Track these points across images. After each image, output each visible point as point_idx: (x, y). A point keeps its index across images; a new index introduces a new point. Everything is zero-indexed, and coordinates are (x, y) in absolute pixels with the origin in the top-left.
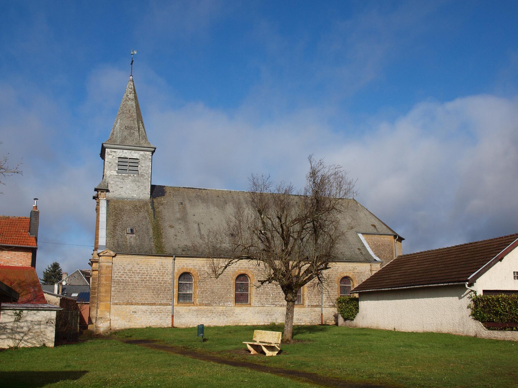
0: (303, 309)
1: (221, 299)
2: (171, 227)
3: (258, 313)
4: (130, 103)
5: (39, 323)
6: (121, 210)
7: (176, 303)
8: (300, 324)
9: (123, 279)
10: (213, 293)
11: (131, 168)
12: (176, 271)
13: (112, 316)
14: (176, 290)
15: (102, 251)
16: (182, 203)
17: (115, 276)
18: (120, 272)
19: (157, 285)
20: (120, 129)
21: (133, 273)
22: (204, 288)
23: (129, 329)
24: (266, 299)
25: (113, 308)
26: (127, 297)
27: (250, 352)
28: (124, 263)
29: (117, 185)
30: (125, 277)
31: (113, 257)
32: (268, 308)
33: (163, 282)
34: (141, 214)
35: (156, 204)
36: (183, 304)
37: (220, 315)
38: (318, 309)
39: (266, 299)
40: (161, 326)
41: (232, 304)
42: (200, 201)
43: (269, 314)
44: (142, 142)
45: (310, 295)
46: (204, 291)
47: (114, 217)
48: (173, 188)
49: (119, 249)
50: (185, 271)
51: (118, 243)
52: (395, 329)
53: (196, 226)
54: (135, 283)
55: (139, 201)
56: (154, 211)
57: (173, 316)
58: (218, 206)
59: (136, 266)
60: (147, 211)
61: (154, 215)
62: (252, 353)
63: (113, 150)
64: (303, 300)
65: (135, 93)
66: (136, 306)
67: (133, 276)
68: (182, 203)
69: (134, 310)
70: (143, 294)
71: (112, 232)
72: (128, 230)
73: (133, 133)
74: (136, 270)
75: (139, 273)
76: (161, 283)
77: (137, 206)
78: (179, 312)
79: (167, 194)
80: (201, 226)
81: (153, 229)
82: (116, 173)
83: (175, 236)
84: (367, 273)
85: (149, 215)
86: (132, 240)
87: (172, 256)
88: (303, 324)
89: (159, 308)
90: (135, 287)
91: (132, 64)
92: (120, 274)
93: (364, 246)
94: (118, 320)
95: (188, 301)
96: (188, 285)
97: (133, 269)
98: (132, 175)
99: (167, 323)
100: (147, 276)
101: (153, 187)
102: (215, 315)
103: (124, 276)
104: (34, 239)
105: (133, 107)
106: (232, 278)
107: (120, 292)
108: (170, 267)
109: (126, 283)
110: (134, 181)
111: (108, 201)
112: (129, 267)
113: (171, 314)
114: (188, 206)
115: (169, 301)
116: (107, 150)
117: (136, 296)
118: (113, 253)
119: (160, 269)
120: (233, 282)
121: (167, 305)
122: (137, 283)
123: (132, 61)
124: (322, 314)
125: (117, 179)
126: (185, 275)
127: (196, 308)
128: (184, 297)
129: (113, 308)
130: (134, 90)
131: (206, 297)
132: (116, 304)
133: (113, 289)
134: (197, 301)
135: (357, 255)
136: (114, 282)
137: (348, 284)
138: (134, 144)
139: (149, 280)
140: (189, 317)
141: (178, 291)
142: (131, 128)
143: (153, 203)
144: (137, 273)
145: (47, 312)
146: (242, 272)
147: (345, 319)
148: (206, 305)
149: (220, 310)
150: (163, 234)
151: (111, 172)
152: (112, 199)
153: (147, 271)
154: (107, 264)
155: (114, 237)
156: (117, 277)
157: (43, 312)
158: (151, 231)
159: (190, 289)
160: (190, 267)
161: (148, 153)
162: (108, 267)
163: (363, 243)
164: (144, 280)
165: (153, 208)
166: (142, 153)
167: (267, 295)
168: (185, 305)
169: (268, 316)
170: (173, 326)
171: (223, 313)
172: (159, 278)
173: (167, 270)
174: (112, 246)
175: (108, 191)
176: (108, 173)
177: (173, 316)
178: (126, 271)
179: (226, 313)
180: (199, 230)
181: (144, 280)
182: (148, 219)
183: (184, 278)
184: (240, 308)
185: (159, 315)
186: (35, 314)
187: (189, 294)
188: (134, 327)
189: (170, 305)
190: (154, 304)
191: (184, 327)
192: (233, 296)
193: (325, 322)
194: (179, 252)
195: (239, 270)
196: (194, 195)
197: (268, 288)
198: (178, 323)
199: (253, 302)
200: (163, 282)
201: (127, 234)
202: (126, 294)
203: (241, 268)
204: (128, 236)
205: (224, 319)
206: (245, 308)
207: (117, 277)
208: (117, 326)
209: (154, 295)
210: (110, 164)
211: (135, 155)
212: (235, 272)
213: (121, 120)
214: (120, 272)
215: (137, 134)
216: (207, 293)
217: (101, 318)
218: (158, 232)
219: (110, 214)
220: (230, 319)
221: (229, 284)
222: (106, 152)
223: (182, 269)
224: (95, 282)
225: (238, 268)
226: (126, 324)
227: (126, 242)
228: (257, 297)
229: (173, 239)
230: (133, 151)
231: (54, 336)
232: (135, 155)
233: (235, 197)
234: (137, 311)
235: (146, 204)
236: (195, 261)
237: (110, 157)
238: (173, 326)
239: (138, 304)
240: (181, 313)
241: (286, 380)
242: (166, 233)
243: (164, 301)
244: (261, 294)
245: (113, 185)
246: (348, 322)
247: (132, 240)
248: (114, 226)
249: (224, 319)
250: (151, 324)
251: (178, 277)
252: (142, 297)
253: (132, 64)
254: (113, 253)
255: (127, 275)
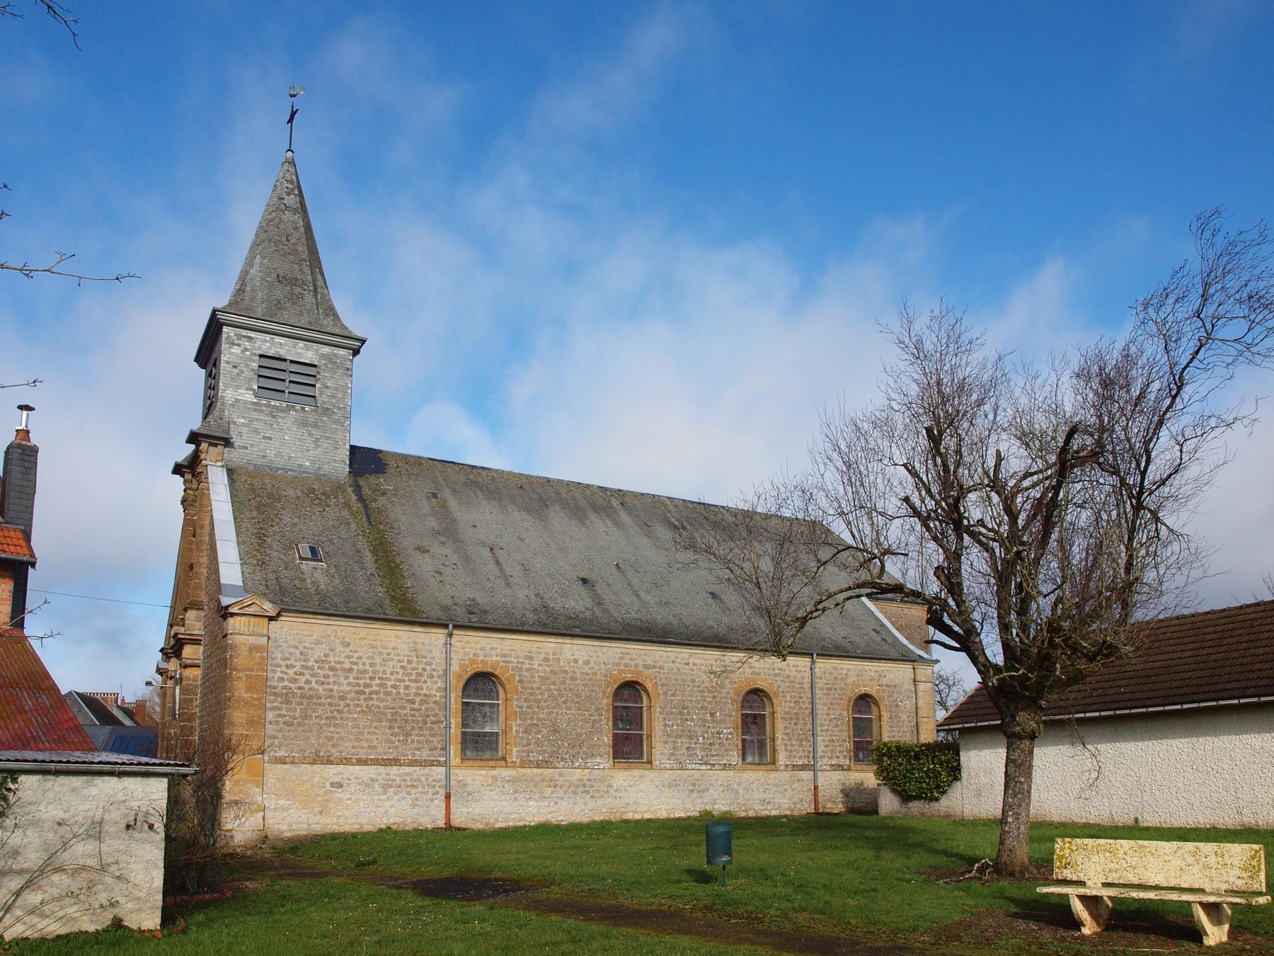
0: (773, 775)
1: (577, 750)
2: (422, 550)
3: (670, 786)
4: (288, 216)
5: (96, 830)
6: (270, 496)
7: (458, 760)
8: (767, 813)
9: (300, 688)
10: (555, 731)
11: (295, 388)
12: (455, 667)
13: (272, 803)
14: (455, 721)
15: (233, 600)
16: (435, 496)
17: (278, 677)
18: (293, 666)
19: (402, 708)
20: (262, 279)
21: (332, 669)
22: (532, 719)
23: (334, 837)
24: (688, 748)
25: (273, 773)
26: (313, 740)
27: (1077, 924)
28: (300, 637)
29: (256, 431)
30: (308, 682)
31: (271, 619)
32: (695, 772)
33: (418, 699)
34: (332, 513)
35: (366, 491)
36: (477, 763)
37: (575, 793)
38: (807, 775)
39: (688, 748)
40: (415, 825)
41: (604, 761)
42: (479, 493)
43: (696, 788)
44: (327, 323)
45: (790, 739)
46: (532, 725)
47: (255, 514)
48: (405, 458)
49: (291, 601)
50: (481, 668)
51: (279, 583)
52: (1136, 820)
53: (486, 553)
54: (337, 701)
55: (319, 478)
56: (366, 507)
57: (448, 797)
58: (527, 510)
59: (339, 648)
60: (347, 505)
61: (370, 522)
62: (1086, 931)
63: (244, 332)
64: (774, 751)
65: (301, 195)
66: (340, 768)
67: (331, 680)
68: (435, 496)
69: (336, 780)
70: (362, 733)
71: (256, 549)
72: (305, 549)
73: (301, 296)
74: (339, 663)
75: (350, 670)
76: (413, 702)
77: (316, 492)
78: (465, 785)
79: (391, 470)
80: (499, 553)
81: (374, 552)
82: (250, 397)
83: (433, 572)
84: (906, 686)
85: (352, 514)
86: (318, 575)
87: (446, 626)
88: (774, 813)
89: (408, 774)
90: (340, 712)
91: (291, 121)
92: (291, 672)
93: (883, 625)
94: (287, 809)
95: (488, 755)
96: (487, 709)
97: (331, 659)
98: (298, 407)
99: (430, 815)
100: (372, 678)
101: (352, 447)
102: (561, 793)
103: (303, 679)
104: (20, 536)
105: (296, 229)
106: (604, 692)
107: (291, 724)
108: (438, 655)
109: (310, 698)
110: (304, 423)
111: (231, 472)
112: (319, 652)
113: (442, 792)
114: (453, 504)
115: (436, 753)
116: (225, 329)
117: (342, 739)
118: (270, 609)
119: (409, 662)
120: (606, 702)
121: (431, 764)
122: (343, 698)
123: (293, 114)
124: (816, 788)
125: (255, 415)
126: (482, 682)
127: (513, 772)
128: (479, 745)
129: (273, 773)
130: (299, 188)
131: (537, 743)
132: (282, 761)
133: (270, 715)
134: (515, 753)
135: (875, 642)
136: (275, 694)
137: (865, 713)
138: (303, 323)
139: (377, 693)
140: (496, 800)
141: (464, 725)
142: (294, 282)
143: (358, 489)
144: (344, 670)
145: (129, 782)
146: (629, 677)
147: (906, 797)
148: (538, 766)
149: (574, 779)
150: (405, 567)
151: (238, 392)
152: (241, 468)
153: (372, 665)
154: (252, 640)
155: (262, 564)
156: (282, 679)
157: (113, 781)
158: (369, 558)
159: (492, 719)
160: (494, 658)
161: (342, 352)
162: (253, 649)
163: (877, 619)
164: (363, 693)
165: (361, 499)
166: (326, 350)
167: (690, 738)
168: (482, 763)
169: (695, 795)
170: (449, 826)
171: (583, 788)
172: (407, 687)
173: (431, 664)
174: (263, 588)
175: (227, 443)
176: (228, 393)
177: (448, 797)
178: (309, 664)
179: (592, 786)
180: (498, 563)
181: (363, 693)
182: (353, 526)
183: (476, 690)
184: (627, 773)
185: (409, 793)
186: (74, 790)
187: (491, 733)
188: (336, 829)
189: (439, 764)
190: (395, 762)
191: (479, 826)
192: (607, 739)
193: (824, 807)
194: (463, 618)
195: (621, 672)
196: (462, 479)
197: (693, 720)
198: (463, 815)
199: (658, 757)
200: (418, 699)
201: (302, 558)
202: (310, 730)
203: (626, 665)
204: (306, 566)
205: (585, 804)
206: (637, 773)
207: (282, 679)
208: (285, 828)
209: (394, 735)
210: (236, 371)
211: (308, 353)
212: (612, 675)
213: (264, 257)
214: (293, 666)
215: (309, 298)
216: (539, 732)
217: (236, 803)
218: (389, 565)
219: (241, 503)
220: (600, 802)
221: (597, 709)
222: (224, 336)
223: (472, 662)
224: (191, 700)
225: (618, 664)
226: (313, 819)
227: (304, 580)
228: (666, 742)
229: (433, 580)
230: (301, 344)
231: (159, 881)
232: (308, 353)
233: (563, 492)
234: (345, 782)
235: (339, 487)
236: (507, 643)
237: (236, 350)
238: (449, 826)
239: (346, 761)
240: (469, 789)
241: (442, 917)
242: (411, 565)
243: (424, 755)
244: (678, 736)
245: (245, 430)
246: (916, 806)
247: (318, 575)
248: (261, 536)
249: (585, 804)
250: (385, 821)
251: (461, 684)
252: (358, 740)
253: (291, 121)
254: (270, 609)
255: (313, 675)
